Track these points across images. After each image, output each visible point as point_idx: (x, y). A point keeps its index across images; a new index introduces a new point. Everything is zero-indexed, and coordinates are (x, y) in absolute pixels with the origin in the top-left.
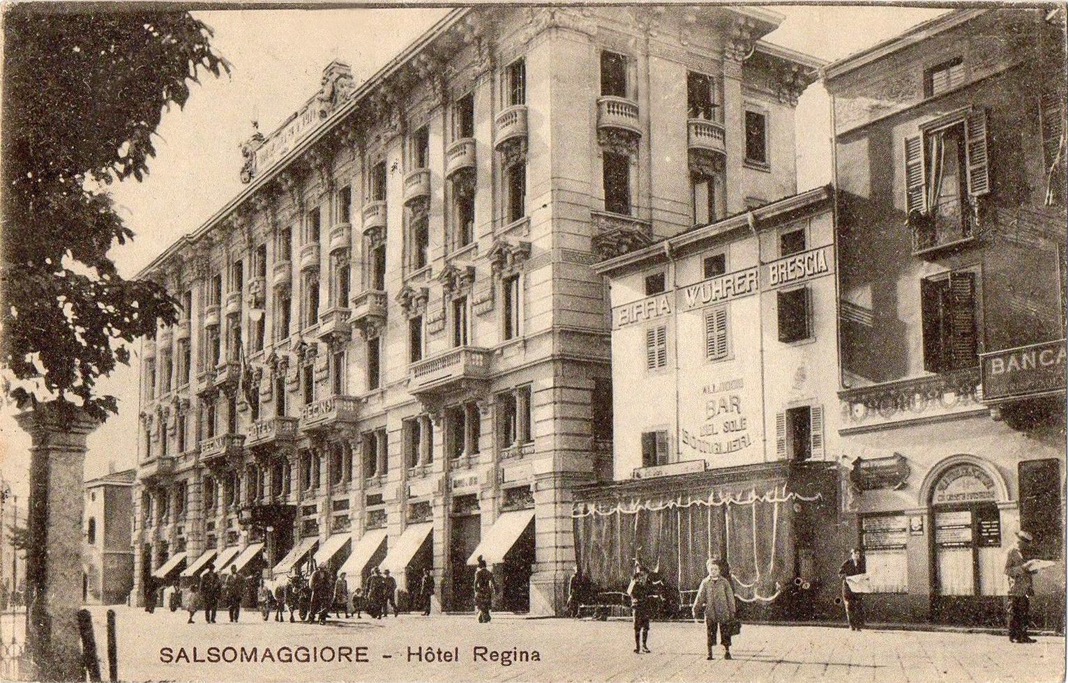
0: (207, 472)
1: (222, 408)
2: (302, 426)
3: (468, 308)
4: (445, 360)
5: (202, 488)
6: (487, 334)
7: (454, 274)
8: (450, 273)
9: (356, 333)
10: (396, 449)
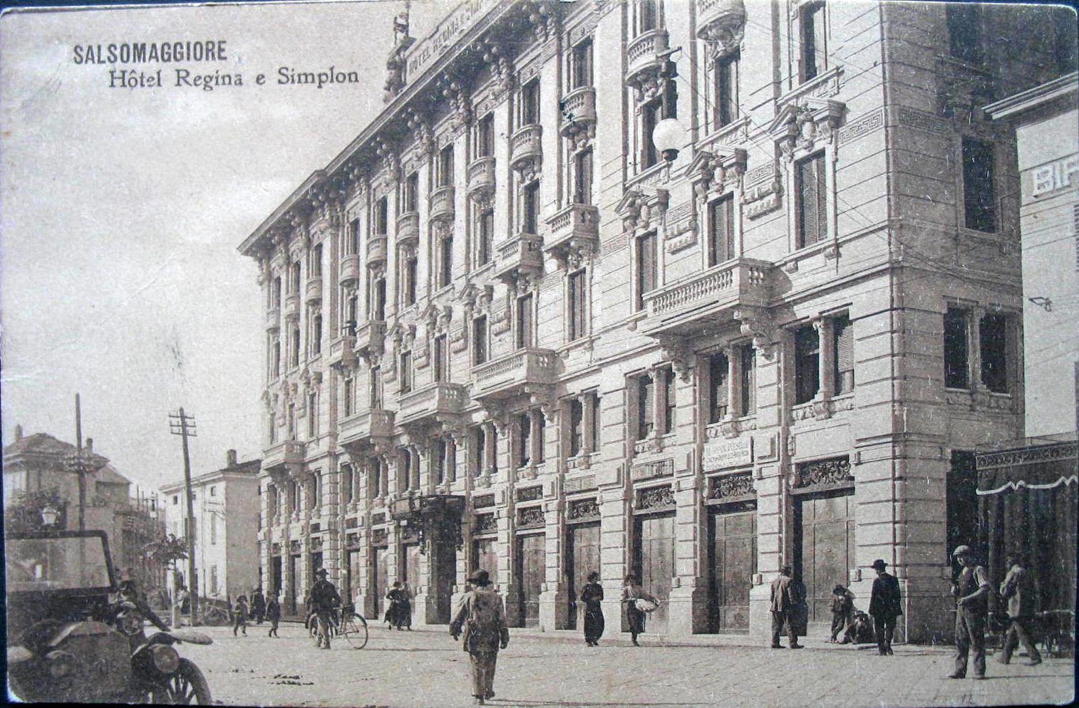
0: (345, 458)
1: (363, 380)
2: (399, 419)
3: (737, 208)
4: (427, 392)
6: (767, 239)
7: (712, 163)
8: (706, 164)
9: (551, 265)
10: (613, 414)
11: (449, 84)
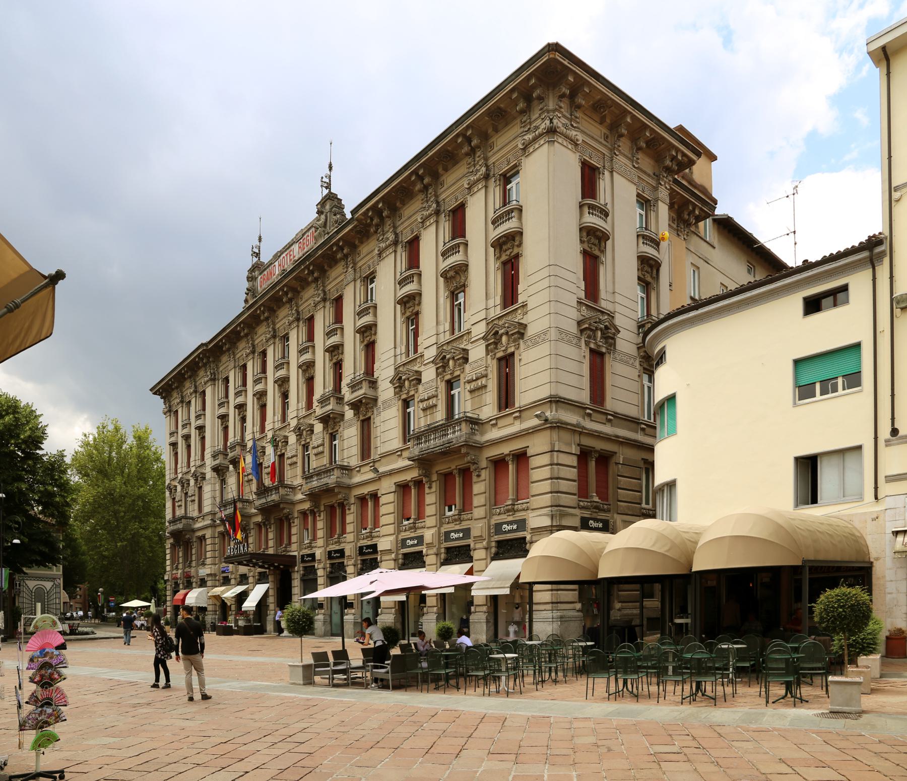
5: (217, 540)
11: (343, 250)
